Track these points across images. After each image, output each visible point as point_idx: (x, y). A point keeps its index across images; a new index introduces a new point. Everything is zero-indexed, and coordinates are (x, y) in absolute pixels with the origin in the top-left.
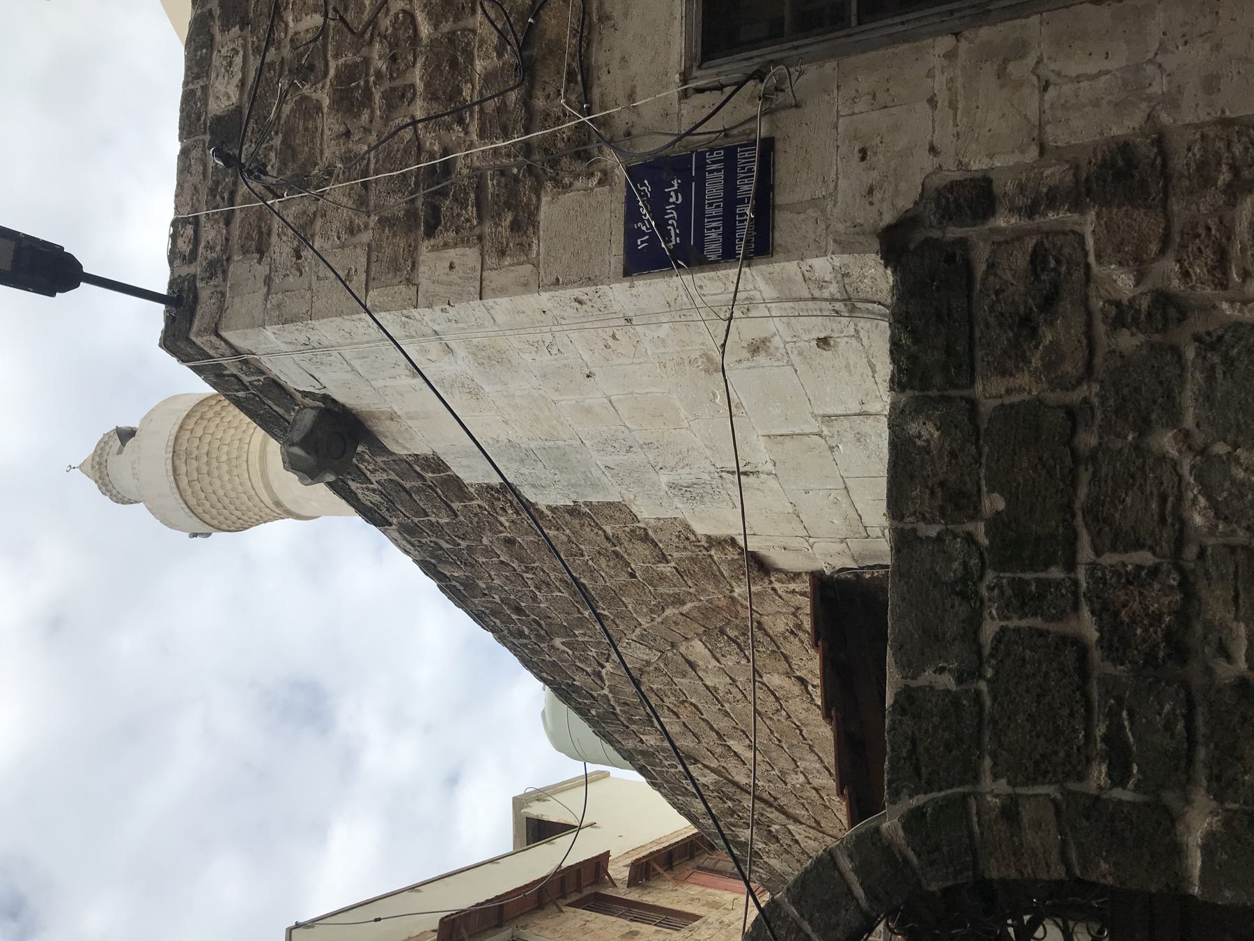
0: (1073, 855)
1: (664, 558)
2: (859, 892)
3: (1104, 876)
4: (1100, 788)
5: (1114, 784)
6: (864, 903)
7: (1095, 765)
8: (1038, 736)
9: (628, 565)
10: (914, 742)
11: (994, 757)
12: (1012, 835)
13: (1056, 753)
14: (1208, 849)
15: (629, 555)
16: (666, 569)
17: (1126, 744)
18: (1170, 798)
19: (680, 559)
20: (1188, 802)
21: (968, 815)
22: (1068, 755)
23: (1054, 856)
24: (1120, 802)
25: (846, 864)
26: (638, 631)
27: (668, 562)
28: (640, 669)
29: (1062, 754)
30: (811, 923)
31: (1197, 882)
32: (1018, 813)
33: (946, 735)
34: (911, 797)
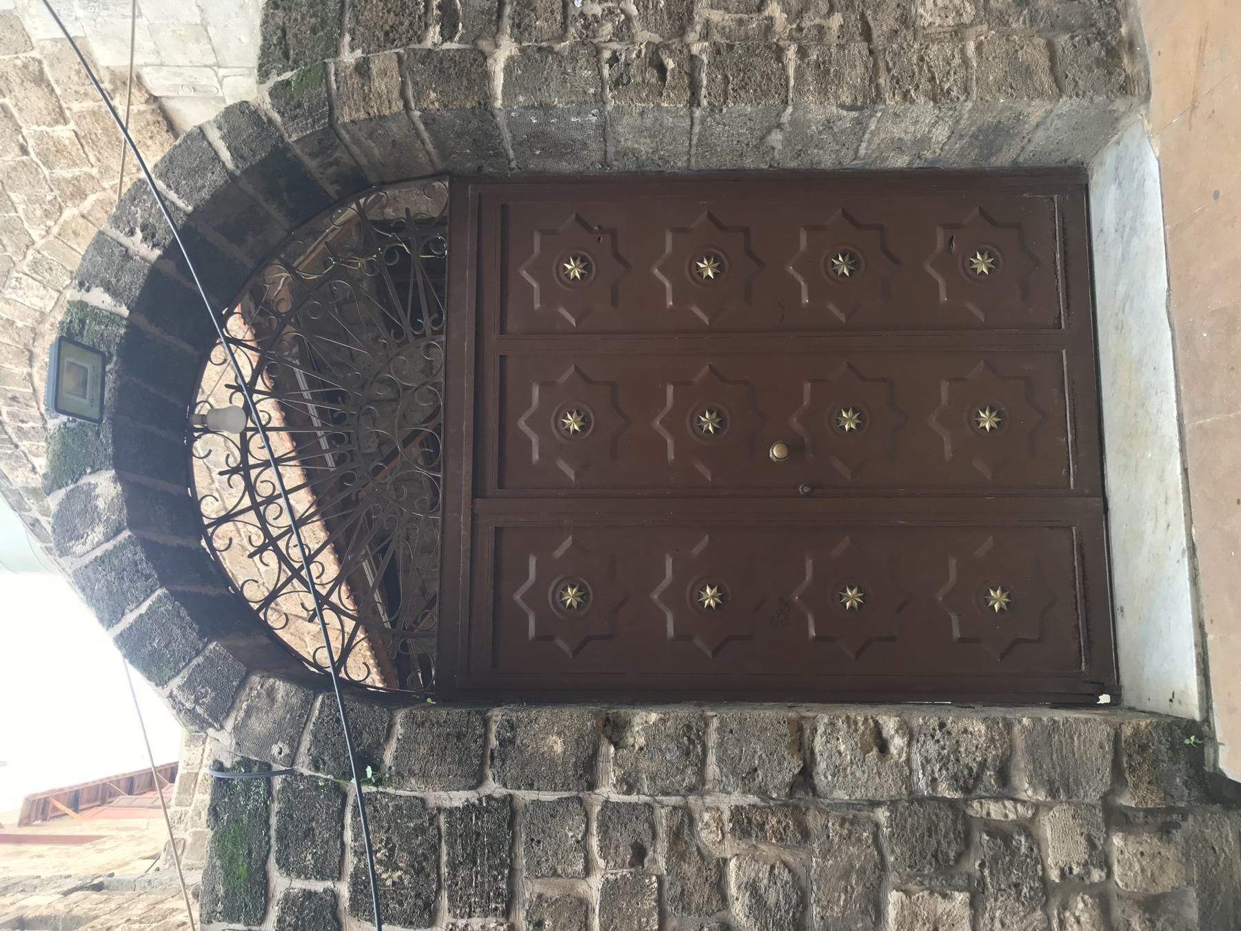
0: (410, 93)
1: (60, 116)
2: (225, 155)
3: (433, 103)
4: (435, 44)
5: (444, 40)
6: (230, 165)
7: (431, 29)
8: (389, 12)
9: (18, 129)
10: (284, 31)
11: (353, 33)
12: (363, 85)
13: (401, 23)
14: (508, 70)
15: (20, 110)
16: (63, 133)
17: (456, 11)
18: (484, 45)
19: (81, 116)
20: (497, 46)
21: (327, 74)
22: (411, 24)
23: (396, 94)
24: (449, 50)
25: (214, 136)
26: (31, 254)
27: (66, 122)
28: (33, 329)
29: (407, 23)
30: (177, 192)
31: (499, 96)
32: (369, 68)
33: (313, 20)
34: (278, 75)
